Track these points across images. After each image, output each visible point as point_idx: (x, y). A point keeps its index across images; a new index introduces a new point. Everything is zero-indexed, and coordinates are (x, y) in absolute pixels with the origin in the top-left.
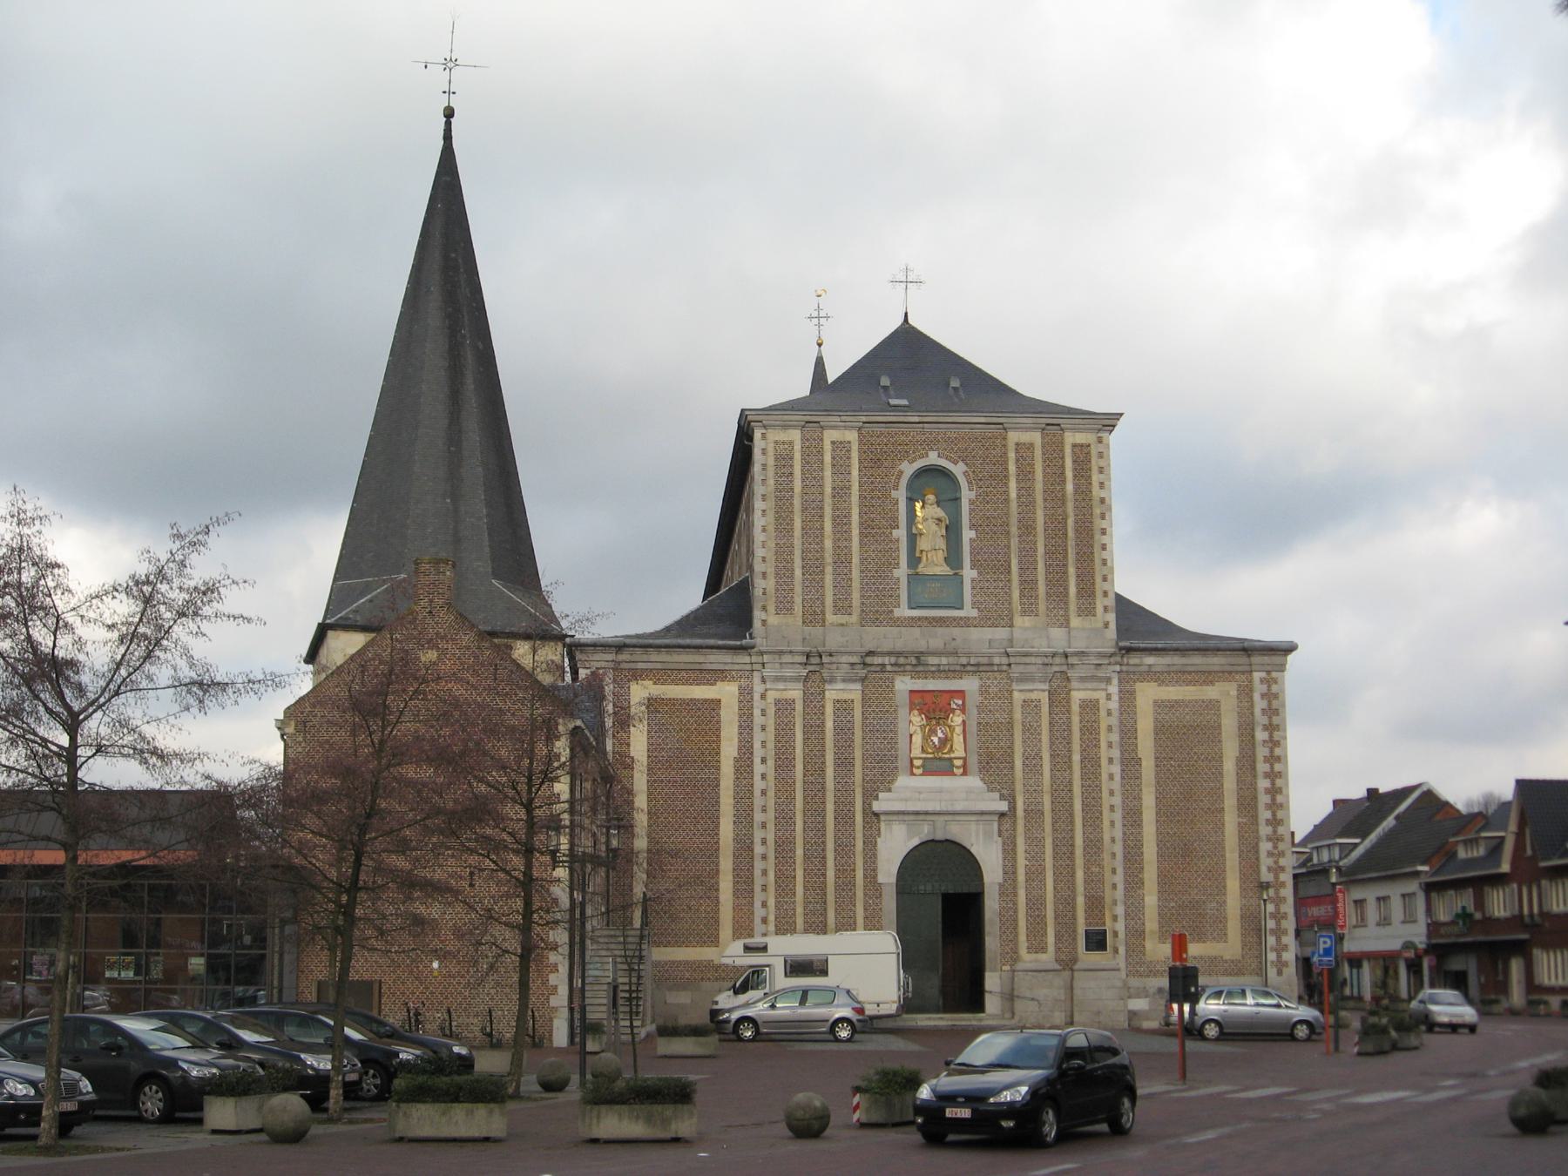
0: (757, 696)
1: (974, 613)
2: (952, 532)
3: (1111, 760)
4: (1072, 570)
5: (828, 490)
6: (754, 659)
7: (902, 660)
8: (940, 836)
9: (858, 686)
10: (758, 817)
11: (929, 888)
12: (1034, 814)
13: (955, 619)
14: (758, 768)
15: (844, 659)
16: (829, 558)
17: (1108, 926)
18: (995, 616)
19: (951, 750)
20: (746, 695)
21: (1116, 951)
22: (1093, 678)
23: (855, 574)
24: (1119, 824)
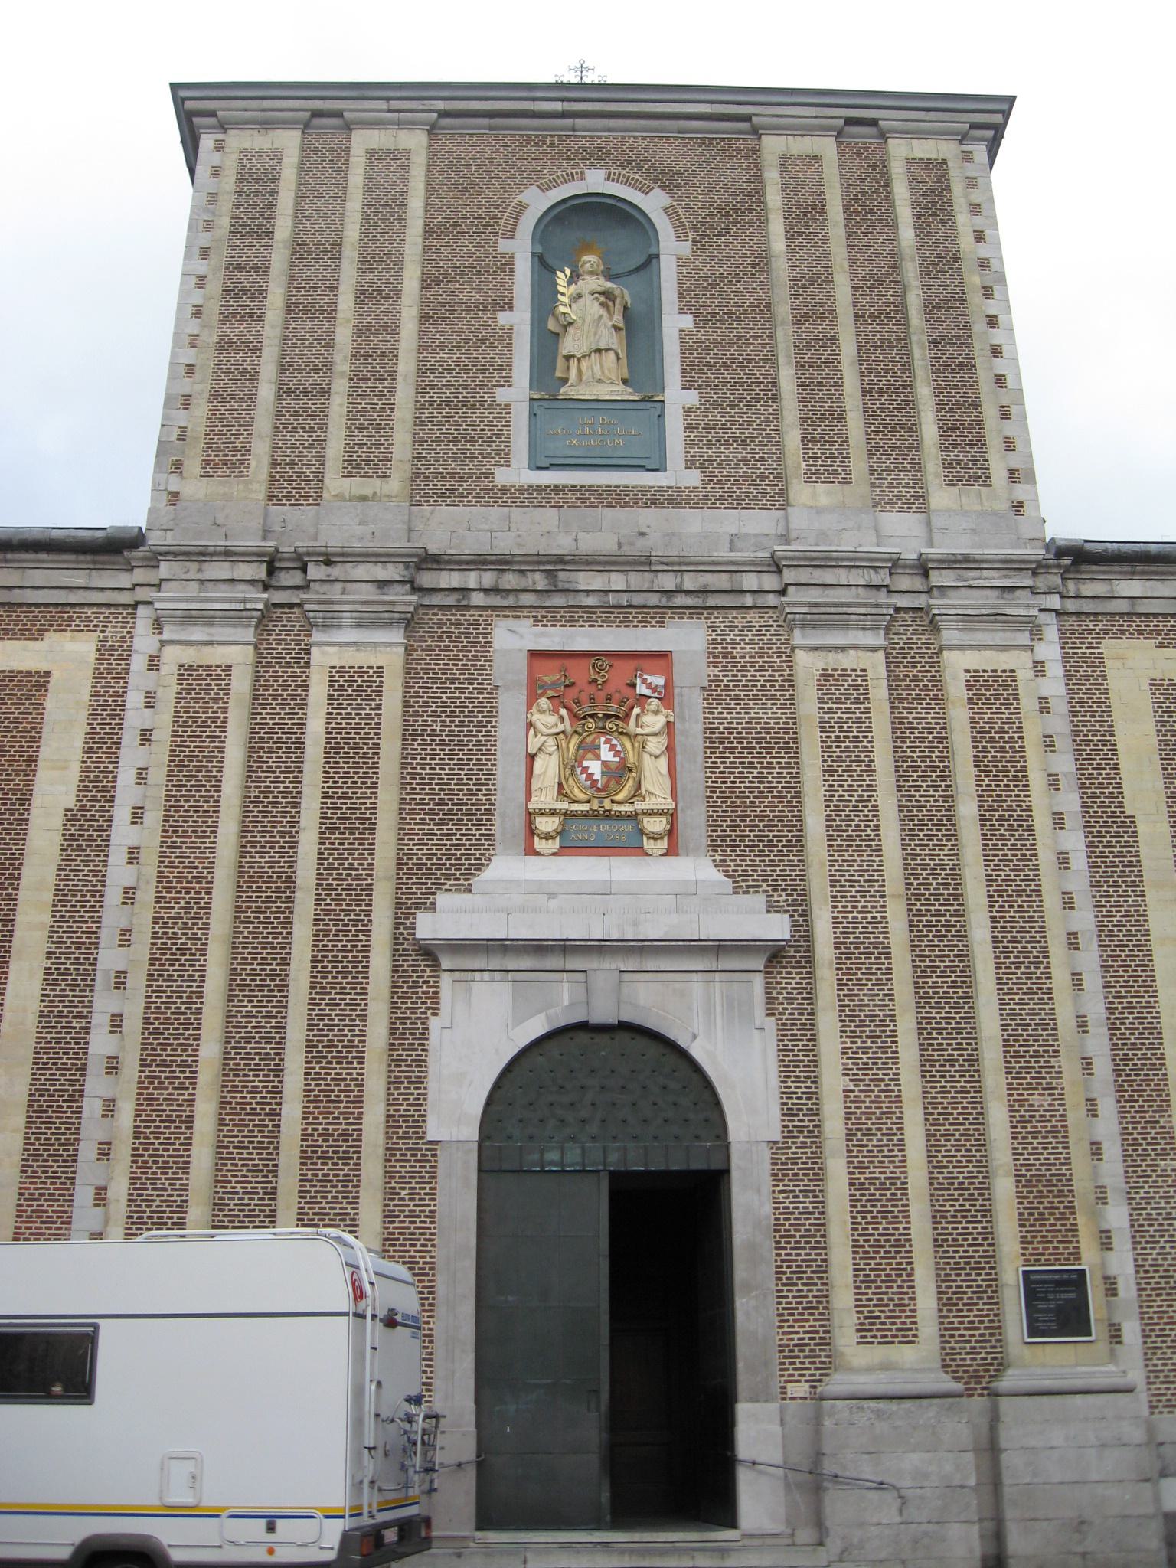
0: (138, 663)
1: (693, 479)
2: (638, 329)
3: (1059, 821)
4: (924, 392)
5: (352, 232)
6: (140, 575)
7: (510, 580)
8: (603, 1013)
9: (397, 636)
10: (109, 958)
11: (573, 1157)
12: (862, 952)
13: (644, 490)
14: (123, 834)
15: (361, 571)
16: (342, 364)
17: (1089, 1258)
18: (744, 478)
19: (637, 794)
20: (113, 665)
21: (1115, 1336)
22: (996, 619)
23: (404, 395)
24: (1093, 981)
